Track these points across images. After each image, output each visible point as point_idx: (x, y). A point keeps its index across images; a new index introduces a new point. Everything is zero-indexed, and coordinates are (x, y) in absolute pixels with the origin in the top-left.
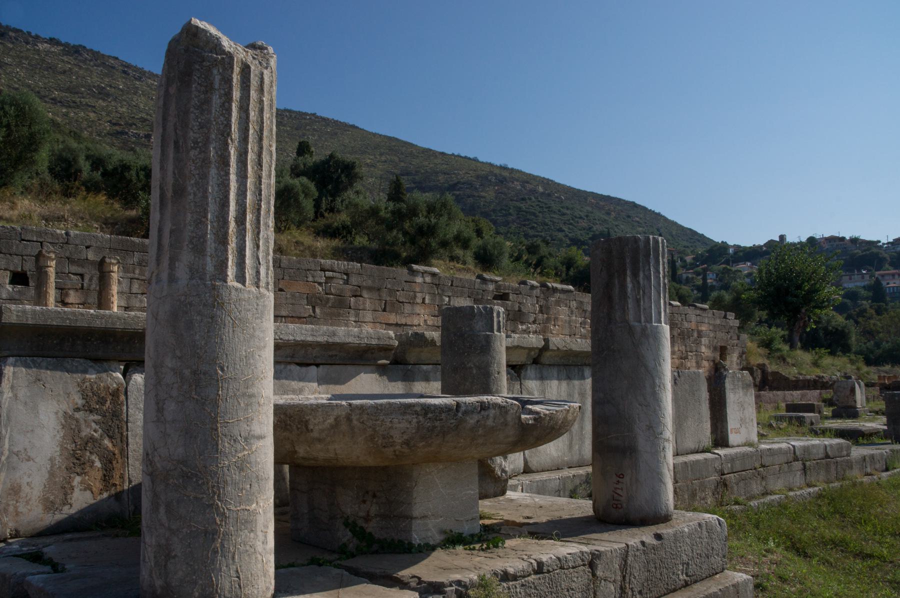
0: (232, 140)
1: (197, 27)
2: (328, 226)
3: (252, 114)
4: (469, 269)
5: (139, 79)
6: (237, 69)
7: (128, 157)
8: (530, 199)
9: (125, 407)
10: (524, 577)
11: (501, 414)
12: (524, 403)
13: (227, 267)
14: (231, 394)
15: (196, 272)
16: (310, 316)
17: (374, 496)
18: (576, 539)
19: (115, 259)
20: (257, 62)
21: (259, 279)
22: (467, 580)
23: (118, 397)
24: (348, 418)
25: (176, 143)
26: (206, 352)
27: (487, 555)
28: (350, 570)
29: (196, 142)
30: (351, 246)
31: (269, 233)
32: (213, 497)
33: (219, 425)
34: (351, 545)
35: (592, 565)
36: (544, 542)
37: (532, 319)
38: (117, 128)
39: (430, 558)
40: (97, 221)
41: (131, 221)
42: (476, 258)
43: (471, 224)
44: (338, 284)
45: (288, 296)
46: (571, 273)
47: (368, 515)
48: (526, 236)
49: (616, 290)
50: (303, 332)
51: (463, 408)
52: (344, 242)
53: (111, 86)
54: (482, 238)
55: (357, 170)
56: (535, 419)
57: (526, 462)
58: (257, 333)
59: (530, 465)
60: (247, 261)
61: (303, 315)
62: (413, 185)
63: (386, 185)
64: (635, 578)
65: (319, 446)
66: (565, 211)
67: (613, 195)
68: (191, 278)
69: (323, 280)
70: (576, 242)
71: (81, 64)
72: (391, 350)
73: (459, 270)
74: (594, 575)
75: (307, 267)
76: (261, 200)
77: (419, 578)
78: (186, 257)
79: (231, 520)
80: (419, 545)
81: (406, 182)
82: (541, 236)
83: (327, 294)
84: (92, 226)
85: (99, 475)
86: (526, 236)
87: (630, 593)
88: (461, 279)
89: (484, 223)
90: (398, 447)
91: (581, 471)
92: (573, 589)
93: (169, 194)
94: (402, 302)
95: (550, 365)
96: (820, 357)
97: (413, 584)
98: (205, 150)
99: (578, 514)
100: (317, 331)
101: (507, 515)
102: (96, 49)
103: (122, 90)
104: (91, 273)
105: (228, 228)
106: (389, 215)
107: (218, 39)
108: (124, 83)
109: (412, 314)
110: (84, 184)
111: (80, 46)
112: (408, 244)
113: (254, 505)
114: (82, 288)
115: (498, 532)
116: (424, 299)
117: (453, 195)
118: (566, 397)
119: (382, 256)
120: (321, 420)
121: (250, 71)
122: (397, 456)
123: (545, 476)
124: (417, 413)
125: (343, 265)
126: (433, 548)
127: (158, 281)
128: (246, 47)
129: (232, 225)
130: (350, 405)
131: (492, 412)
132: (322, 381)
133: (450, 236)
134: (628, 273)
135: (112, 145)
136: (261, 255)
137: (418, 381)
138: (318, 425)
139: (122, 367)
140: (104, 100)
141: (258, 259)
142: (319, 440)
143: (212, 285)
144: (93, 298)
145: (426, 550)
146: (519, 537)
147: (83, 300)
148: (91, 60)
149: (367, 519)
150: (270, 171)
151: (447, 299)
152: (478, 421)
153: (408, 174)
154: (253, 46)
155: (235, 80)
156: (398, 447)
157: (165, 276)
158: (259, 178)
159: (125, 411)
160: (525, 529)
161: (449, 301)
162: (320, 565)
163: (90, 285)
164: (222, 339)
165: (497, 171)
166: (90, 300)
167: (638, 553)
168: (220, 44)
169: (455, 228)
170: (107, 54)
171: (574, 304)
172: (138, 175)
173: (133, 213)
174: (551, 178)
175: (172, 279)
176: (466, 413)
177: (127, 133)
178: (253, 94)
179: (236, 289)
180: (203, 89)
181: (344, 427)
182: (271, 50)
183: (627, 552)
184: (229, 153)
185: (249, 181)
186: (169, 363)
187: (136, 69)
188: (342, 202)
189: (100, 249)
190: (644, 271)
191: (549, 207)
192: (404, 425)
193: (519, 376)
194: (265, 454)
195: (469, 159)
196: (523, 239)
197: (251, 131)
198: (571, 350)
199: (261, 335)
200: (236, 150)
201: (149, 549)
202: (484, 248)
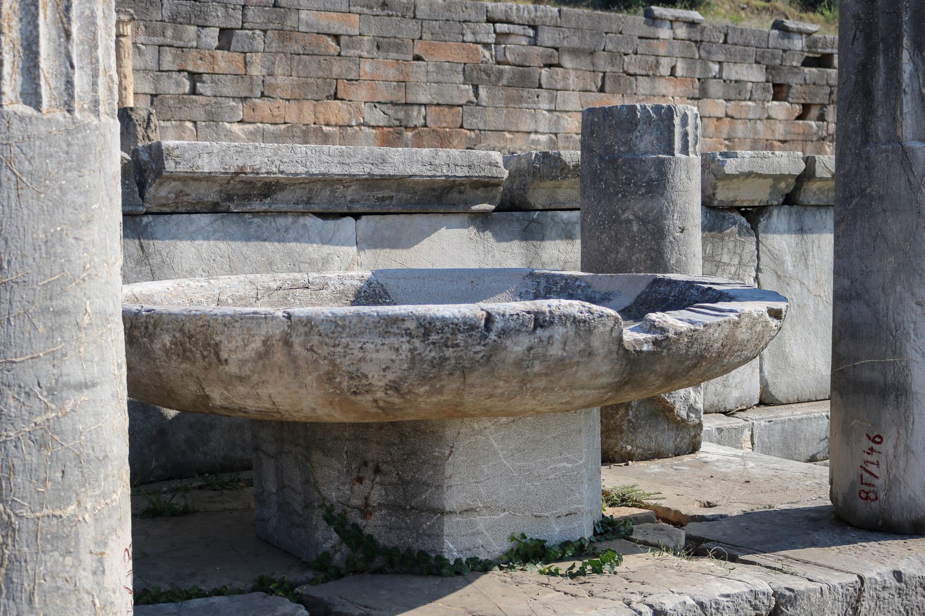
14: (17, 310)
16: (470, 102)
17: (377, 471)
21: (71, 96)
34: (338, 556)
45: (431, 68)
47: (367, 505)
49: (881, 78)
56: (656, 342)
57: (765, 387)
58: (71, 196)
59: (773, 390)
61: (457, 101)
65: (242, 389)
69: (491, 39)
72: (497, 185)
75: (462, 16)
79: (24, 536)
80: (458, 561)
83: (498, 63)
90: (380, 394)
94: (635, 75)
95: (818, 207)
96: (374, 507)
115: (627, 536)
116: (673, 68)
123: (799, 412)
124: (408, 333)
126: (485, 567)
131: (558, 331)
132: (362, 243)
134: (906, 41)
138: (237, 351)
142: (241, 379)
149: (366, 510)
151: (716, 67)
152: (530, 349)
156: (380, 394)
161: (721, 70)
167: (885, 594)
176: (504, 333)
179: (22, 119)
181: (279, 356)
192: (386, 355)
193: (754, 228)
199: (80, 200)
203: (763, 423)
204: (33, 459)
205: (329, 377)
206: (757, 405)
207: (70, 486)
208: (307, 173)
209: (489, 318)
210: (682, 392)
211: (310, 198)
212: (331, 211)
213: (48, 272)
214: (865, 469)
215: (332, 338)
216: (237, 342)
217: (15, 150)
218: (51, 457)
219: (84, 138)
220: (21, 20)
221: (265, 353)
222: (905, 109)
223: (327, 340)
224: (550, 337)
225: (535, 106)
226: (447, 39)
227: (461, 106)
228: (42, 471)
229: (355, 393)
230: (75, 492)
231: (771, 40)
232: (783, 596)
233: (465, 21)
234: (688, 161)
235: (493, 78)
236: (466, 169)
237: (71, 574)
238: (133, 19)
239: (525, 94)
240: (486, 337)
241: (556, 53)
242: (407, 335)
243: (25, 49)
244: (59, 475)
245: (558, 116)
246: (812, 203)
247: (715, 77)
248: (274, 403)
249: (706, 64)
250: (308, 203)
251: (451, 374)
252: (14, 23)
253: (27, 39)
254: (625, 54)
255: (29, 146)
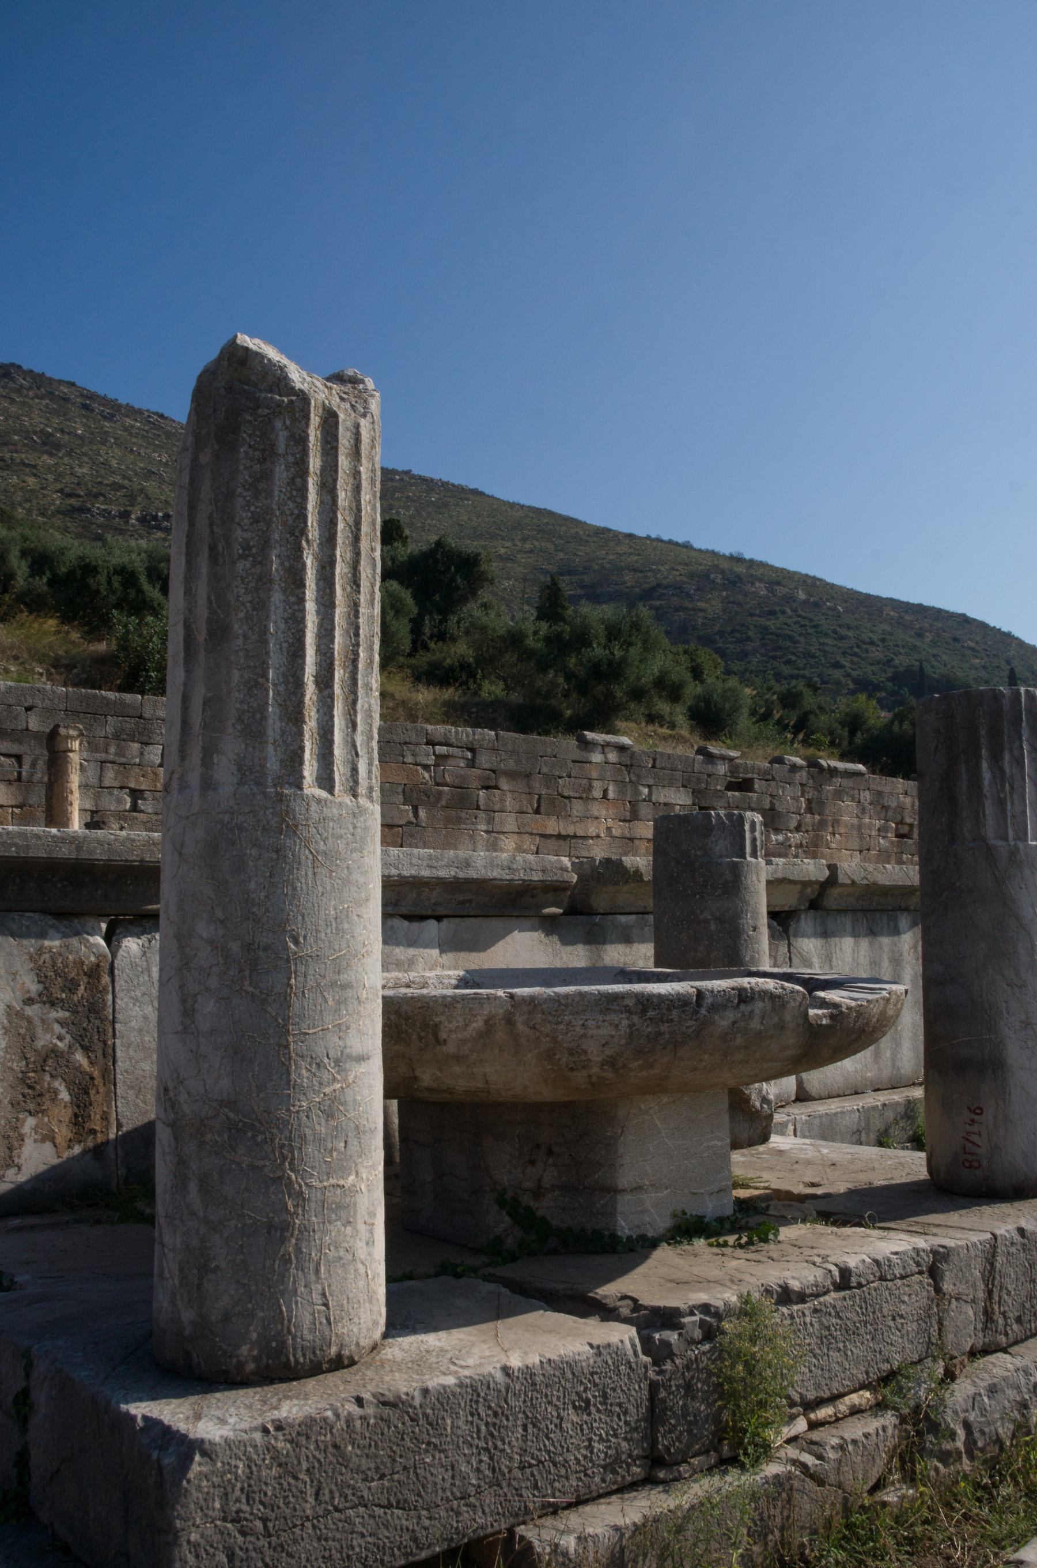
0: (308, 541)
1: (247, 349)
2: (435, 666)
3: (342, 495)
4: (681, 736)
5: (110, 418)
6: (315, 420)
7: (94, 552)
8: (783, 612)
9: (110, 997)
10: (817, 1296)
11: (773, 1009)
12: (812, 985)
13: (301, 762)
14: (311, 983)
15: (249, 773)
17: (550, 1152)
18: (902, 1224)
19: (75, 728)
20: (348, 406)
21: (356, 782)
22: (720, 1304)
23: (99, 979)
24: (509, 1021)
25: (212, 548)
26: (267, 910)
27: (750, 1256)
28: (508, 1283)
29: (247, 547)
30: (476, 699)
31: (373, 701)
32: (282, 1164)
33: (291, 1038)
34: (510, 1240)
35: (934, 1273)
36: (848, 1230)
37: (793, 824)
38: (72, 501)
39: (650, 1262)
40: (40, 662)
41: (100, 660)
42: (692, 717)
43: (683, 658)
44: (456, 768)
46: (858, 739)
48: (778, 676)
50: (414, 861)
51: (709, 1000)
52: (465, 694)
53: (62, 431)
54: (702, 681)
55: (484, 567)
56: (832, 1017)
59: (807, 1086)
60: (337, 752)
61: (397, 822)
62: (579, 592)
63: (534, 593)
64: (1009, 1293)
65: (457, 1069)
66: (844, 632)
67: (927, 602)
68: (241, 783)
69: (431, 760)
70: (864, 686)
71: (14, 396)
72: (565, 889)
73: (665, 738)
74: (938, 1290)
75: (403, 738)
76: (358, 644)
77: (635, 1301)
78: (231, 746)
79: (313, 1205)
80: (629, 1238)
81: (567, 586)
82: (804, 677)
83: (438, 784)
84: (32, 671)
85: (67, 1115)
86: (778, 676)
87: (1001, 1321)
88: (669, 756)
89: (705, 656)
90: (596, 1070)
91: (897, 1097)
92: (902, 1317)
93: (201, 636)
94: (569, 798)
95: (839, 911)
97: (625, 1311)
98: (262, 560)
99: (901, 1177)
100: (437, 859)
101: (775, 1180)
102: (38, 370)
103: (80, 437)
104: (35, 753)
105: (303, 695)
106: (539, 645)
107: (282, 368)
108: (85, 425)
109: (585, 818)
110: (20, 599)
111: (13, 365)
112: (574, 695)
113: (352, 1177)
114: (19, 779)
115: (764, 1212)
116: (605, 792)
117: (651, 607)
118: (882, 972)
119: (530, 717)
120: (462, 1023)
121: (337, 423)
122: (593, 1084)
123: (833, 1106)
124: (628, 1011)
125: (465, 733)
126: (653, 1244)
127: (184, 786)
128: (328, 379)
129: (310, 689)
130: (512, 996)
131: (758, 1006)
132: (447, 945)
133: (647, 679)
134: (984, 753)
135: (65, 530)
136: (359, 740)
137: (612, 942)
138: (455, 1032)
139: (104, 926)
140: (51, 455)
141: (354, 746)
142: (458, 1058)
143: (277, 793)
144: (37, 797)
145: (641, 1247)
146: (804, 1221)
147: (20, 799)
148: (30, 388)
149: (538, 1193)
150: (373, 593)
151: (646, 791)
152: (734, 1023)
153: (570, 573)
154: (339, 378)
155: (312, 439)
156: (596, 1070)
157: (194, 778)
158: (355, 606)
159: (110, 1003)
160: (809, 1205)
162: (457, 1276)
163: (32, 775)
164: (295, 889)
165: (725, 565)
166: (33, 800)
167: (1013, 1250)
168: (286, 378)
169: (657, 665)
170: (57, 376)
171: (866, 796)
172: (109, 582)
173: (102, 647)
174: (819, 575)
175: (208, 785)
176: (713, 1008)
177: (89, 510)
178: (344, 462)
179: (319, 801)
180: (258, 454)
181: (501, 1035)
182: (370, 383)
183: (994, 1247)
184: (304, 564)
185: (338, 611)
186: (204, 930)
187: (105, 401)
188: (458, 622)
189: (49, 711)
190: (1011, 750)
191: (816, 626)
192: (606, 1031)
193: (786, 931)
194: (370, 1086)
195: (677, 544)
196: (773, 683)
197: (341, 526)
198: (875, 884)
199: (361, 880)
200: (316, 558)
201: (171, 1256)
202: (706, 699)
203: (803, 1117)
204: (322, 1129)
205: (550, 1055)
206: (794, 1102)
207: (351, 1156)
208: (399, 875)
209: (700, 994)
210: (757, 1085)
211: (398, 900)
212: (417, 913)
213: (337, 947)
214: (968, 1140)
215: (554, 1016)
216: (458, 1022)
217: (313, 830)
218: (336, 1128)
219: (365, 821)
220: (318, 710)
221: (487, 1033)
222: (988, 812)
223: (550, 1018)
224: (751, 1012)
225: (473, 827)
226: (388, 760)
227: (401, 826)
228: (329, 1141)
229: (572, 1069)
230: (354, 1162)
231: (696, 765)
232: (938, 1253)
233: (405, 743)
234: (758, 864)
235: (432, 799)
236: (540, 874)
237: (351, 1244)
238: (82, 734)
239: (463, 815)
240: (698, 1012)
241: (494, 775)
242: (626, 1011)
243: (321, 738)
244: (342, 1145)
245: (495, 838)
246: (834, 908)
247: (644, 800)
248: (487, 1082)
249: (636, 788)
250: (396, 905)
251: (664, 1048)
252: (313, 714)
253: (323, 729)
254: (560, 777)
255: (324, 828)
